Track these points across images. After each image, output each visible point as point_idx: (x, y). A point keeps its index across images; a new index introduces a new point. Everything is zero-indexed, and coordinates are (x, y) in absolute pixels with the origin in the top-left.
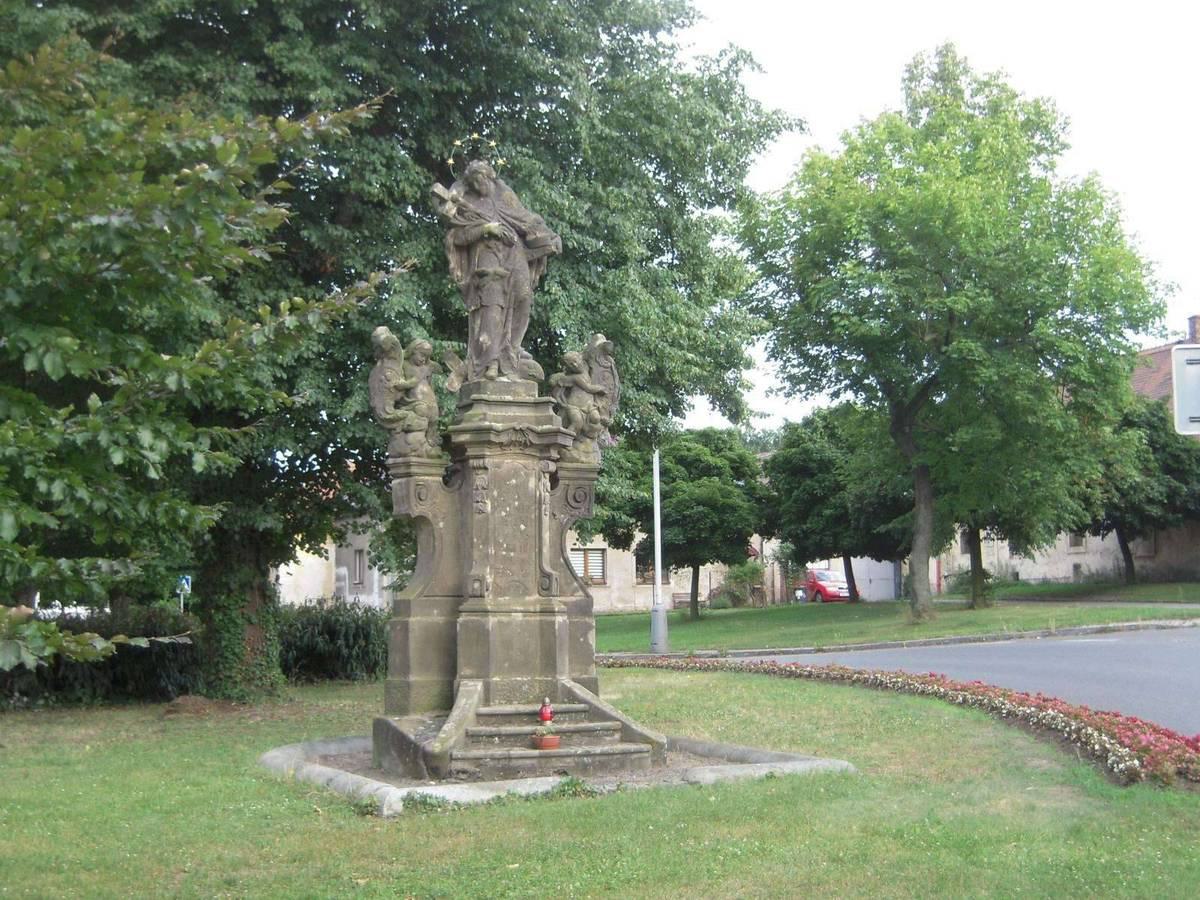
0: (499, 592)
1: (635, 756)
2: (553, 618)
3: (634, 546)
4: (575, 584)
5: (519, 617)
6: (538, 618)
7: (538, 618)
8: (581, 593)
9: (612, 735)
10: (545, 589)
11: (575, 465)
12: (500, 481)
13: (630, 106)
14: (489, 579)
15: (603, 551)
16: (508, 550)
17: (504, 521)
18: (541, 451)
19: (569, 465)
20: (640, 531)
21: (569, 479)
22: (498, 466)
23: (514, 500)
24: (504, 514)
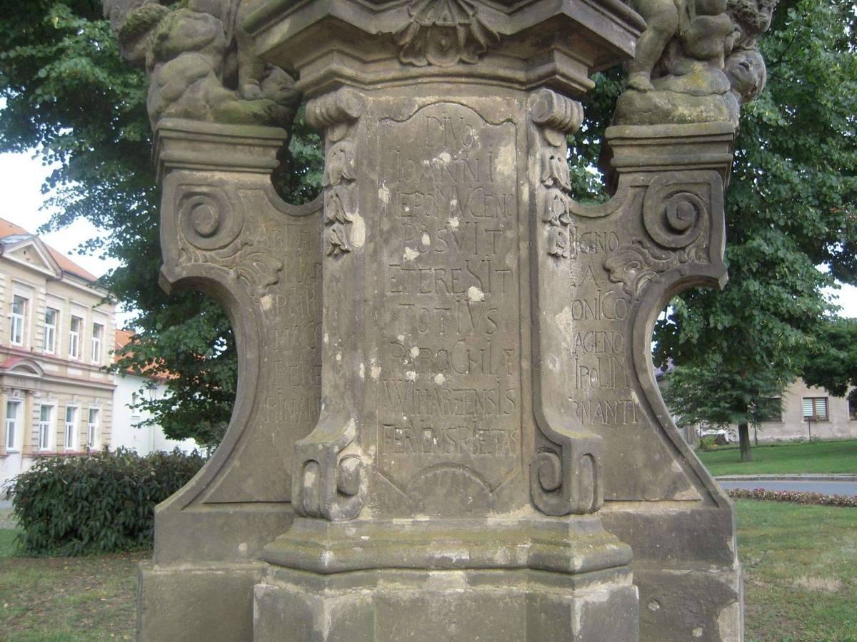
0: (395, 500)
2: (565, 595)
3: (847, 394)
4: (677, 466)
5: (455, 583)
6: (522, 588)
7: (522, 588)
8: (693, 492)
10: (552, 492)
11: (661, 129)
12: (400, 160)
14: (357, 458)
15: (826, 399)
16: (427, 364)
17: (410, 276)
18: (528, 62)
19: (646, 130)
20: (852, 385)
21: (648, 168)
22: (393, 115)
24: (411, 254)
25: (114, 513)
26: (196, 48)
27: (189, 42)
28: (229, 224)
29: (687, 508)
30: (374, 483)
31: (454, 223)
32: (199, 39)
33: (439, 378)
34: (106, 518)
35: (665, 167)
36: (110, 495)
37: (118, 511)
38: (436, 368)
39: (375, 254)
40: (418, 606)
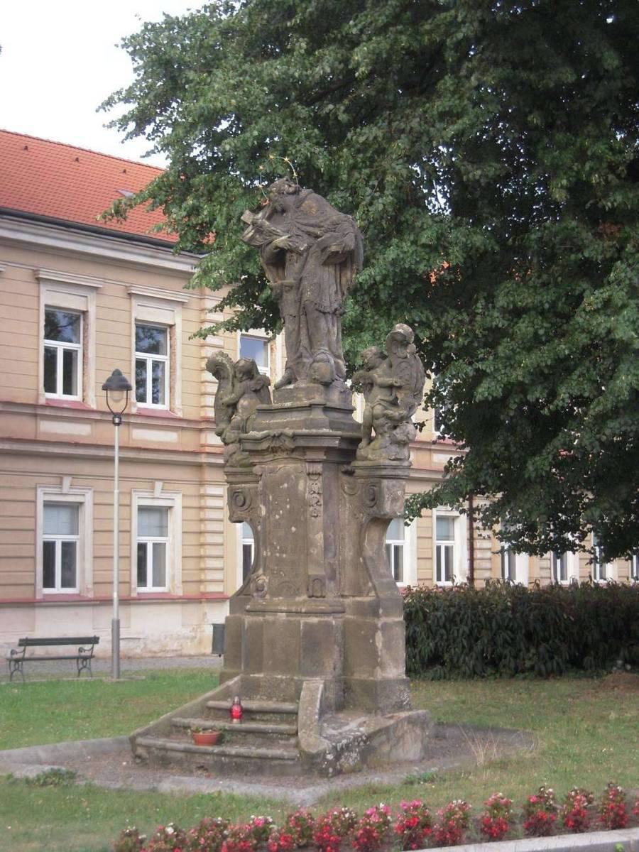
1: (276, 762)
9: (288, 739)
13: (199, 83)
17: (277, 524)
22: (272, 471)
23: (287, 503)
24: (277, 517)
25: (473, 642)
26: (232, 443)
27: (231, 441)
28: (248, 502)
29: (372, 599)
30: (269, 588)
31: (288, 506)
32: (233, 440)
33: (284, 556)
34: (463, 647)
35: (368, 477)
36: (466, 625)
37: (477, 640)
38: (283, 553)
39: (269, 517)
40: (274, 623)
